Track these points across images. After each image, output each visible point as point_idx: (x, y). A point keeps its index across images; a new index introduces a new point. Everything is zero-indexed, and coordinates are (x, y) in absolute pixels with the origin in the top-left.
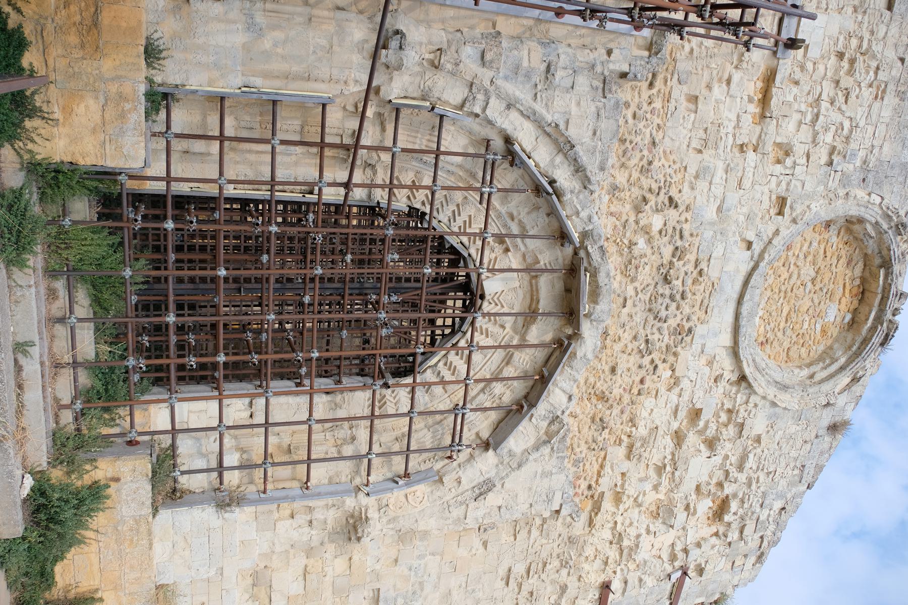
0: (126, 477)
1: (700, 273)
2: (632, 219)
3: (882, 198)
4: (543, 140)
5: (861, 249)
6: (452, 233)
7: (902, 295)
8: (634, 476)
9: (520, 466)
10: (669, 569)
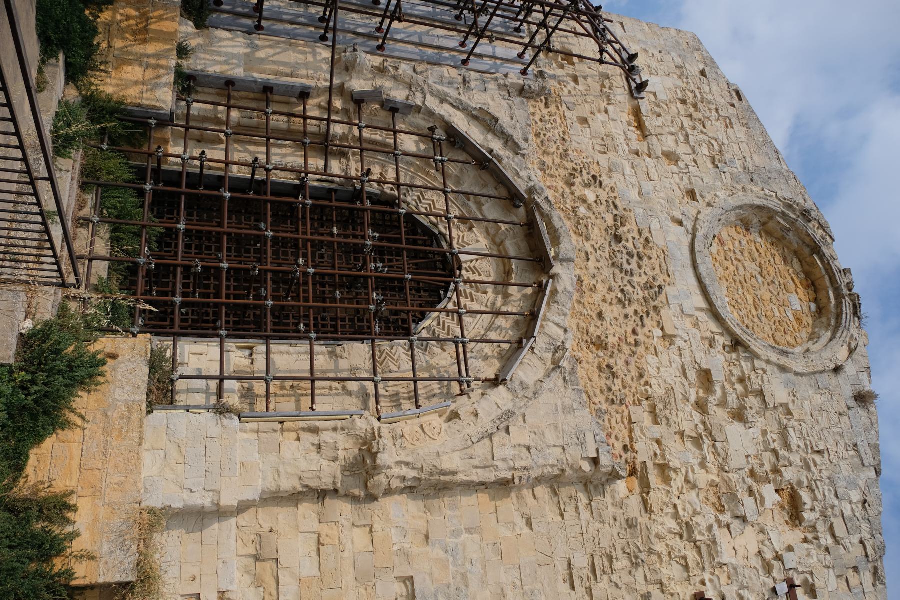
5: (788, 248)
6: (420, 214)
7: (846, 272)
9: (535, 394)
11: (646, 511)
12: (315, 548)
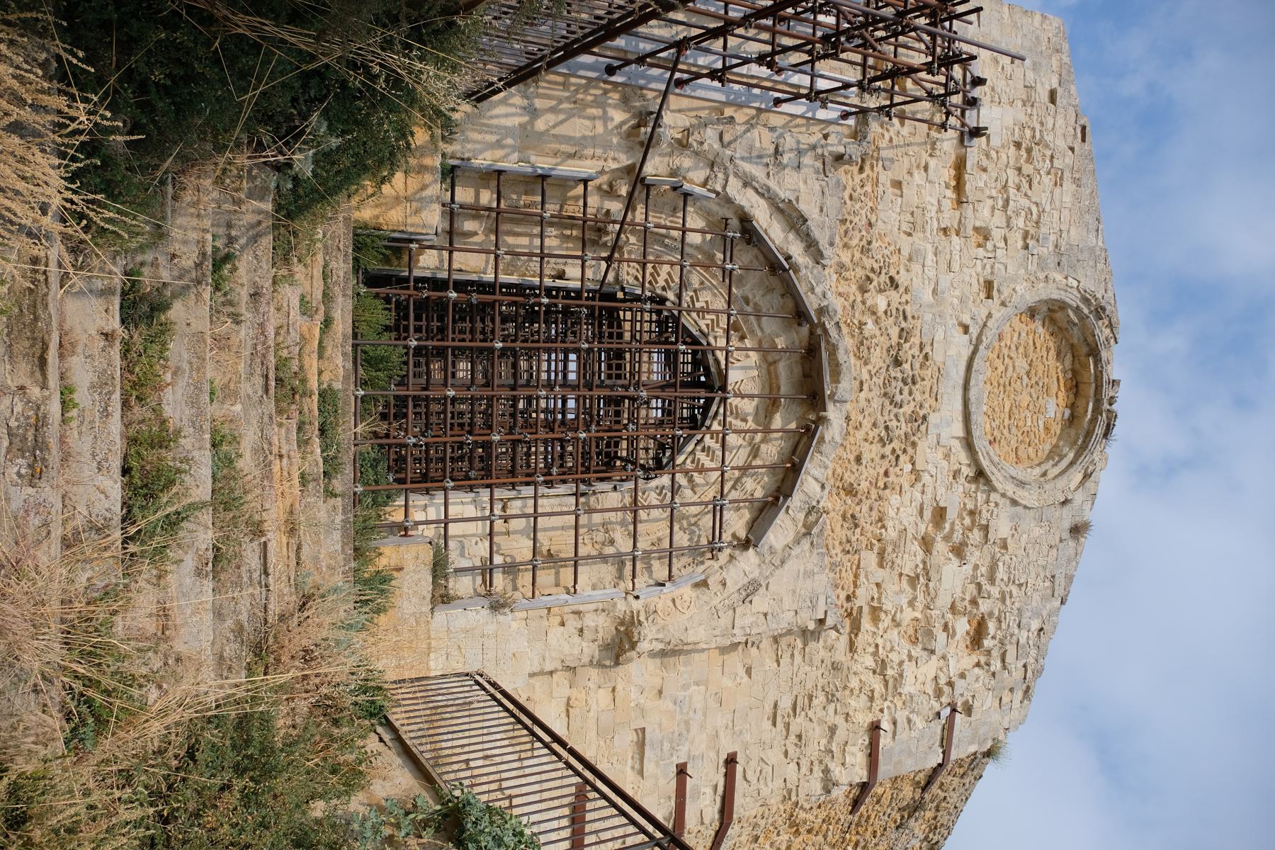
0: (409, 566)
1: (926, 357)
2: (859, 299)
3: (1079, 282)
4: (777, 216)
5: (1067, 340)
7: (1115, 383)
8: (891, 587)
9: (783, 562)
10: (937, 707)
11: (851, 650)
12: (564, 709)
